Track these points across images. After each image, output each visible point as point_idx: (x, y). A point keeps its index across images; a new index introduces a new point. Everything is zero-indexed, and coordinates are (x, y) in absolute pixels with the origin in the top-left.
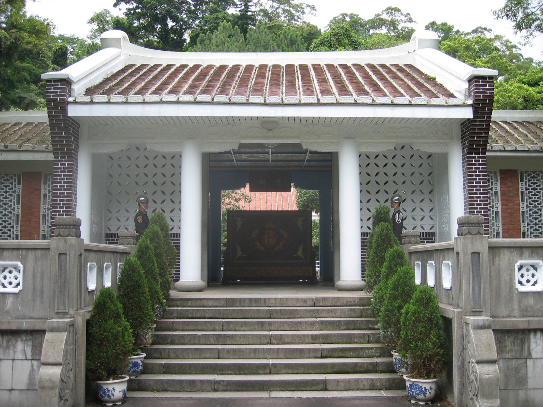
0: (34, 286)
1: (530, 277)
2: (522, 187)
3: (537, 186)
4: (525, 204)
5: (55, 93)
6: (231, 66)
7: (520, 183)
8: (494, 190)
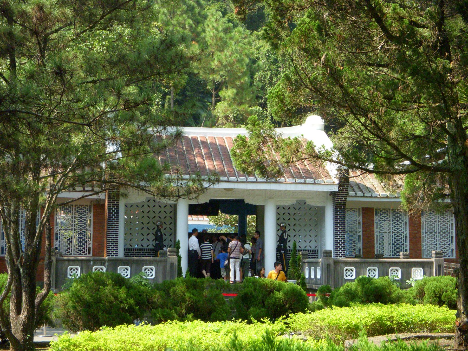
1: (350, 274)
7: (375, 216)
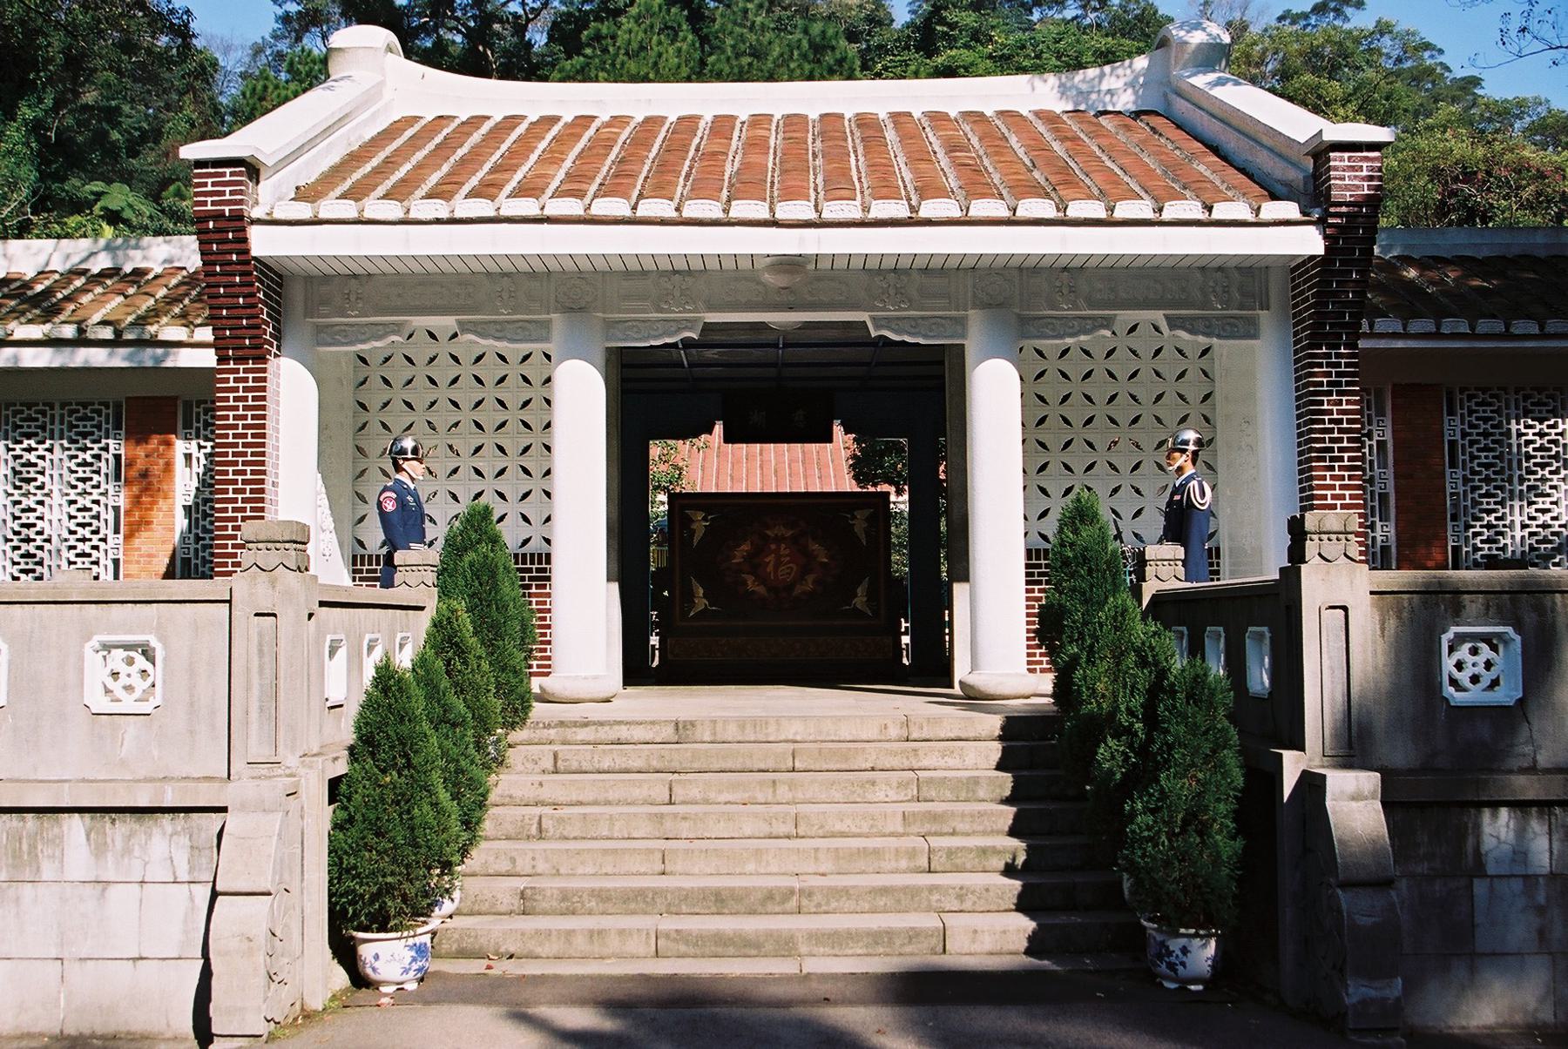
0: (192, 696)
1: (1480, 669)
2: (1452, 428)
3: (1493, 427)
4: (1460, 472)
5: (207, 196)
6: (673, 118)
7: (1446, 418)
8: (1376, 438)
